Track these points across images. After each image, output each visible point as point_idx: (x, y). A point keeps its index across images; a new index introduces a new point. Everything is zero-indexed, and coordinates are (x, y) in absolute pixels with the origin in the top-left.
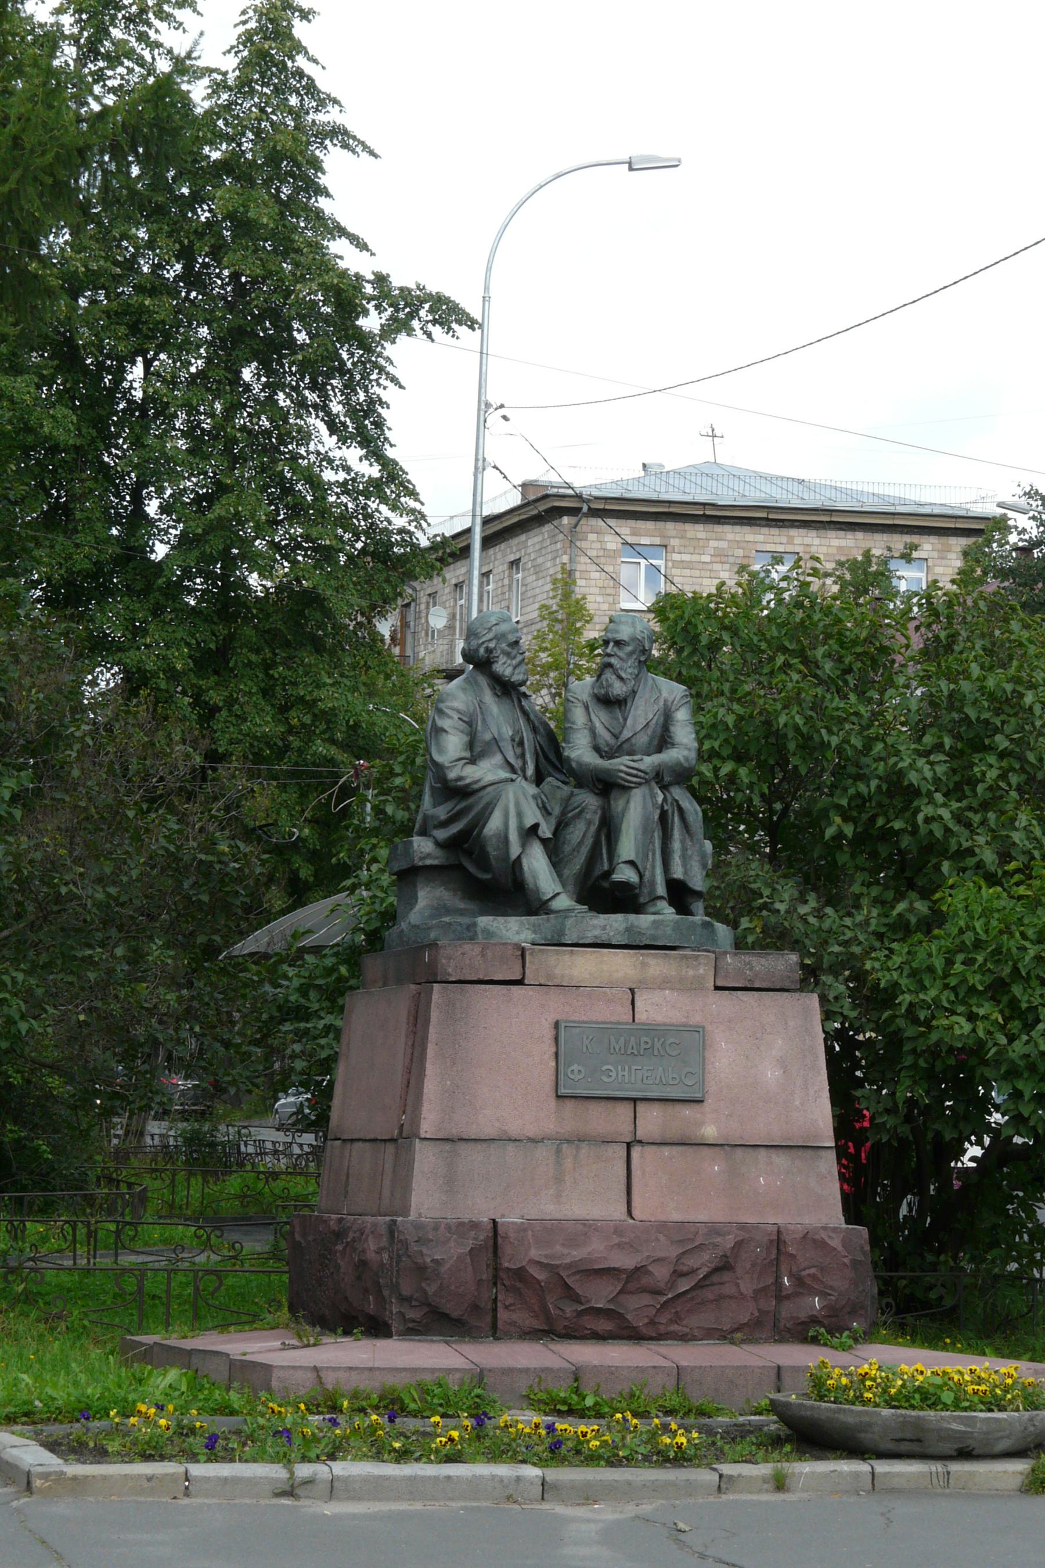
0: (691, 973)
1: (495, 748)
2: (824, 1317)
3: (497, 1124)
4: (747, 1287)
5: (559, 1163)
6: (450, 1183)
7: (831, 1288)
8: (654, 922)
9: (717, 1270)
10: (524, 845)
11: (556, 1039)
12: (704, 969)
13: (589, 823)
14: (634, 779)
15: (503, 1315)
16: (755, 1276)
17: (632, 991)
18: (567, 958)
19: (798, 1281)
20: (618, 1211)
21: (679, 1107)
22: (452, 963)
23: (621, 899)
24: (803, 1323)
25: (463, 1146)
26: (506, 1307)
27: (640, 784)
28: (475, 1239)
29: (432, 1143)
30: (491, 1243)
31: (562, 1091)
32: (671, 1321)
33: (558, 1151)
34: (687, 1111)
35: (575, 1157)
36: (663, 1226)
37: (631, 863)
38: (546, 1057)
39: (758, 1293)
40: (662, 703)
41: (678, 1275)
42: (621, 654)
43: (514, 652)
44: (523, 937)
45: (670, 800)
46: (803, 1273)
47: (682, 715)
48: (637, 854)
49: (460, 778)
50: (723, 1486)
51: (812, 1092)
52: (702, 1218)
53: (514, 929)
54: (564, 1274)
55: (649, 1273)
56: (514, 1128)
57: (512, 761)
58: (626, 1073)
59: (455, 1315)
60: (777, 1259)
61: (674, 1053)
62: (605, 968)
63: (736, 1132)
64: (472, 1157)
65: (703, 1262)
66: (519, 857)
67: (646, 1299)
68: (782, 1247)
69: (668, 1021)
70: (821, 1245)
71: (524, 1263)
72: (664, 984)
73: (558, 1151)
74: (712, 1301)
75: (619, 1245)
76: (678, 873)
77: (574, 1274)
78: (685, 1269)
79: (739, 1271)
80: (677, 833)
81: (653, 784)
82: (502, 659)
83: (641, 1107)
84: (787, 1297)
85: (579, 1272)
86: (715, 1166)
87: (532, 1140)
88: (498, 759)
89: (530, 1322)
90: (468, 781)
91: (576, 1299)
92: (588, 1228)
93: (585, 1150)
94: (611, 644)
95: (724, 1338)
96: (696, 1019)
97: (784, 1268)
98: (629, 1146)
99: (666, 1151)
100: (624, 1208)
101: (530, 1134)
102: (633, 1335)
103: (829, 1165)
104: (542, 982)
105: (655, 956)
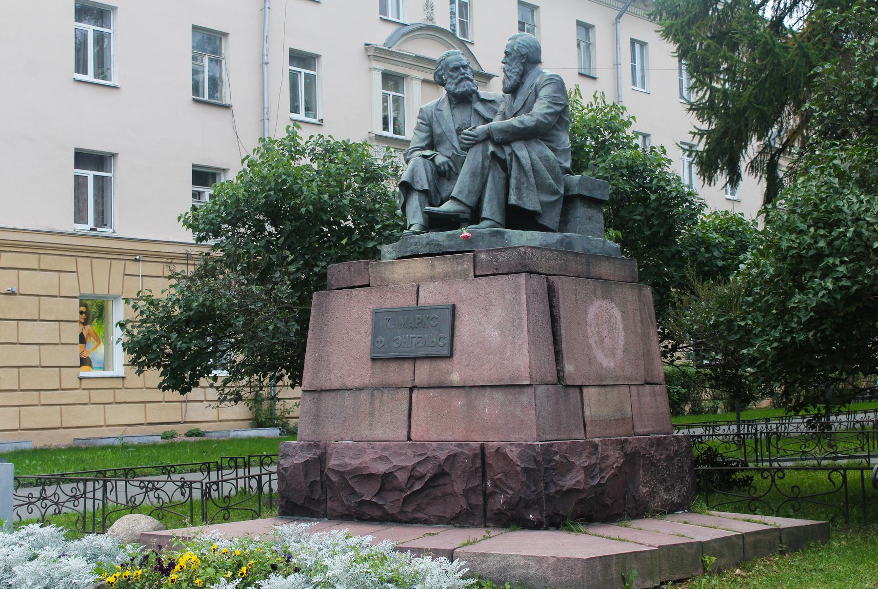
0: (460, 268)
3: (340, 379)
4: (459, 487)
5: (372, 403)
8: (448, 236)
12: (466, 264)
16: (466, 479)
19: (495, 485)
25: (323, 393)
27: (473, 145)
32: (416, 510)
33: (372, 395)
34: (443, 365)
35: (381, 399)
39: (466, 493)
43: (455, 75)
51: (517, 346)
54: (347, 477)
55: (395, 477)
56: (349, 383)
64: (328, 401)
65: (428, 470)
70: (505, 456)
72: (432, 279)
73: (372, 395)
75: (380, 458)
76: (513, 200)
78: (418, 474)
79: (454, 476)
80: (514, 173)
82: (449, 80)
83: (418, 363)
86: (459, 401)
87: (359, 389)
89: (341, 510)
91: (354, 493)
93: (387, 394)
95: (448, 523)
99: (431, 392)
101: (357, 385)
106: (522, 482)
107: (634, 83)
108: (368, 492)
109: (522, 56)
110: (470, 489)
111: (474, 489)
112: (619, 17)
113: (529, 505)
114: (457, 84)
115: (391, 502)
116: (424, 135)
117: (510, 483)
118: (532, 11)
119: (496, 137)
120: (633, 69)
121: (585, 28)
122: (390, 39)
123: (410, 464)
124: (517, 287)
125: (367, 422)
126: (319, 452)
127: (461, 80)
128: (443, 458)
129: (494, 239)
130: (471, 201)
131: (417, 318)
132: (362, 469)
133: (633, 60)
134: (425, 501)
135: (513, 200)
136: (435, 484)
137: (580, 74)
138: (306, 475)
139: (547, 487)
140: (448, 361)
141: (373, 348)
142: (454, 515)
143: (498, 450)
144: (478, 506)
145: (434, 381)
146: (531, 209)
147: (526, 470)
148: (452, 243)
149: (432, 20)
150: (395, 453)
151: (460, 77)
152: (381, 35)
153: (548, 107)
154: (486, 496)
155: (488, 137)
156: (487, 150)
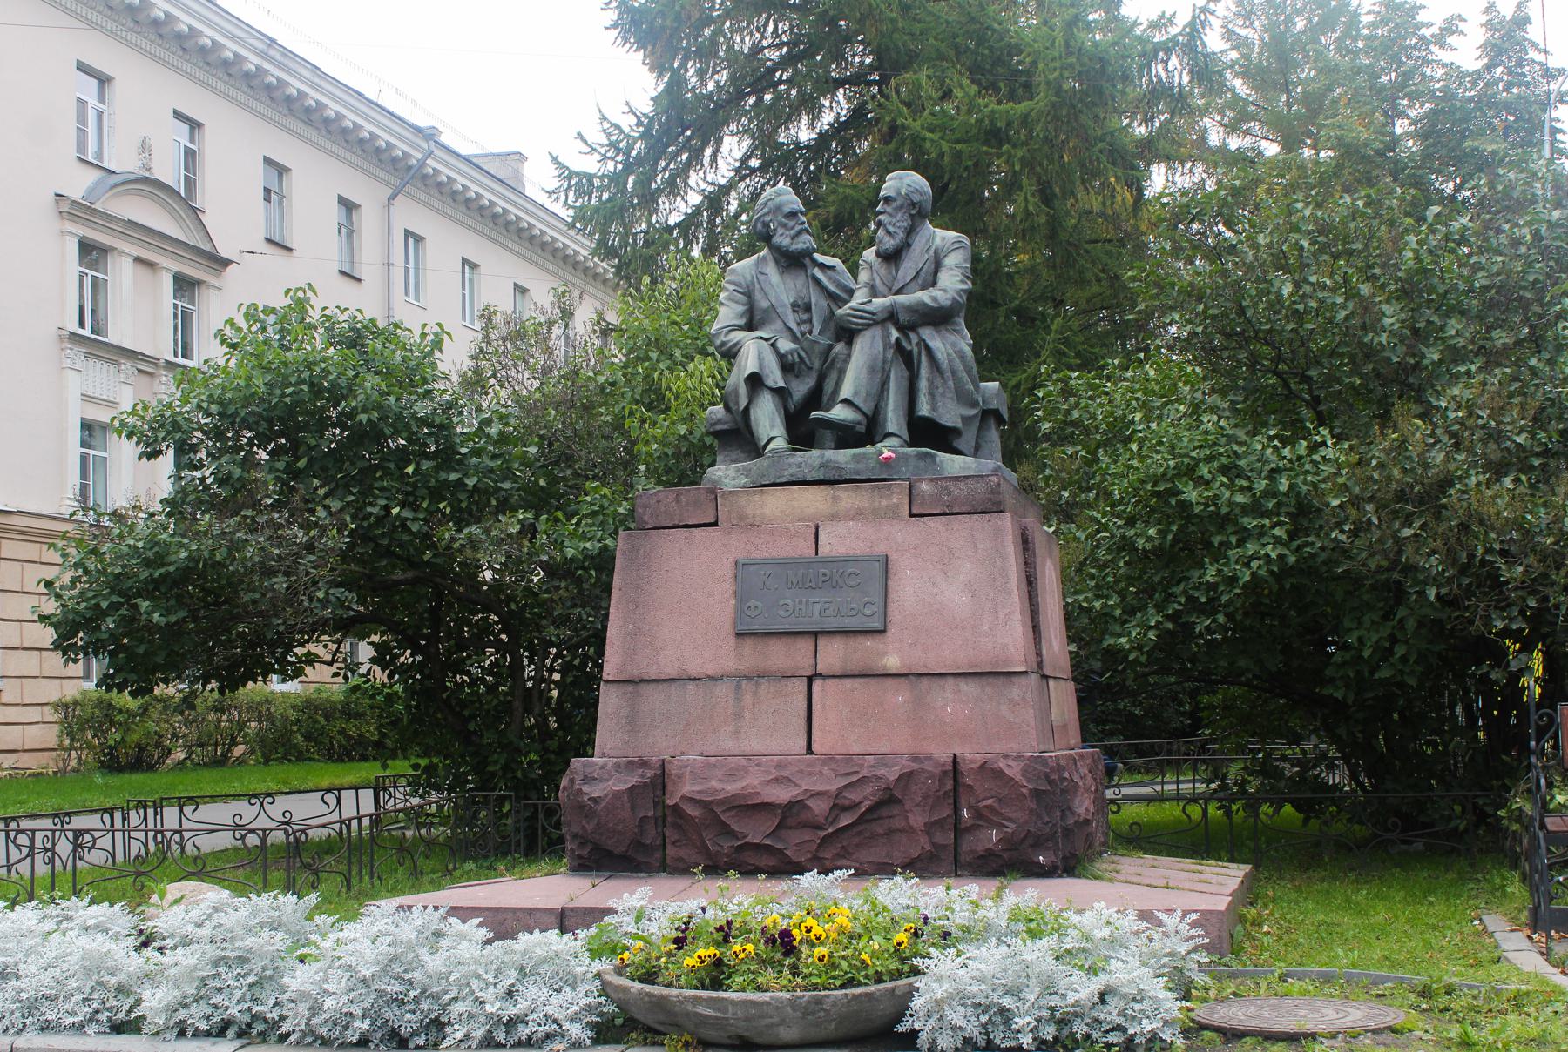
0: (884, 503)
1: (774, 315)
3: (677, 664)
4: (917, 819)
5: (738, 699)
6: (632, 724)
8: (854, 455)
12: (898, 498)
15: (671, 851)
18: (757, 498)
19: (977, 814)
22: (648, 511)
24: (982, 857)
25: (644, 686)
27: (869, 326)
33: (738, 687)
34: (869, 643)
35: (755, 693)
39: (930, 828)
40: (932, 252)
41: (838, 808)
42: (889, 209)
43: (791, 223)
51: (1001, 616)
54: (718, 810)
55: (808, 807)
56: (694, 668)
59: (619, 850)
61: (852, 583)
62: (796, 504)
64: (653, 698)
65: (865, 796)
66: (747, 409)
67: (807, 835)
70: (999, 774)
72: (834, 517)
73: (738, 687)
74: (882, 836)
75: (776, 779)
76: (924, 409)
77: (729, 810)
78: (847, 802)
79: (908, 805)
80: (924, 371)
82: (780, 231)
83: (822, 641)
84: (969, 830)
85: (733, 808)
86: (899, 696)
87: (712, 678)
88: (778, 325)
91: (732, 834)
93: (764, 685)
96: (881, 549)
98: (810, 680)
99: (848, 683)
101: (710, 672)
105: (846, 489)
106: (1031, 811)
107: (407, 293)
108: (756, 832)
109: (913, 205)
110: (936, 822)
111: (939, 823)
112: (393, 197)
113: (1039, 843)
114: (793, 238)
115: (794, 843)
116: (741, 308)
117: (1006, 811)
118: (280, 175)
119: (903, 318)
120: (407, 270)
121: (348, 206)
122: (91, 191)
123: (834, 787)
124: (998, 533)
125: (731, 728)
126: (650, 773)
127: (799, 233)
129: (922, 464)
130: (868, 408)
131: (822, 573)
132: (744, 796)
133: (407, 261)
134: (857, 840)
135: (924, 409)
137: (341, 272)
138: (633, 808)
139: (1063, 817)
140: (878, 637)
141: (740, 613)
143: (983, 766)
144: (945, 846)
145: (852, 667)
146: (950, 424)
147: (1037, 794)
148: (861, 466)
149: (149, 170)
150: (801, 772)
151: (798, 228)
152: (79, 183)
153: (962, 282)
154: (959, 830)
155: (891, 316)
156: (889, 336)
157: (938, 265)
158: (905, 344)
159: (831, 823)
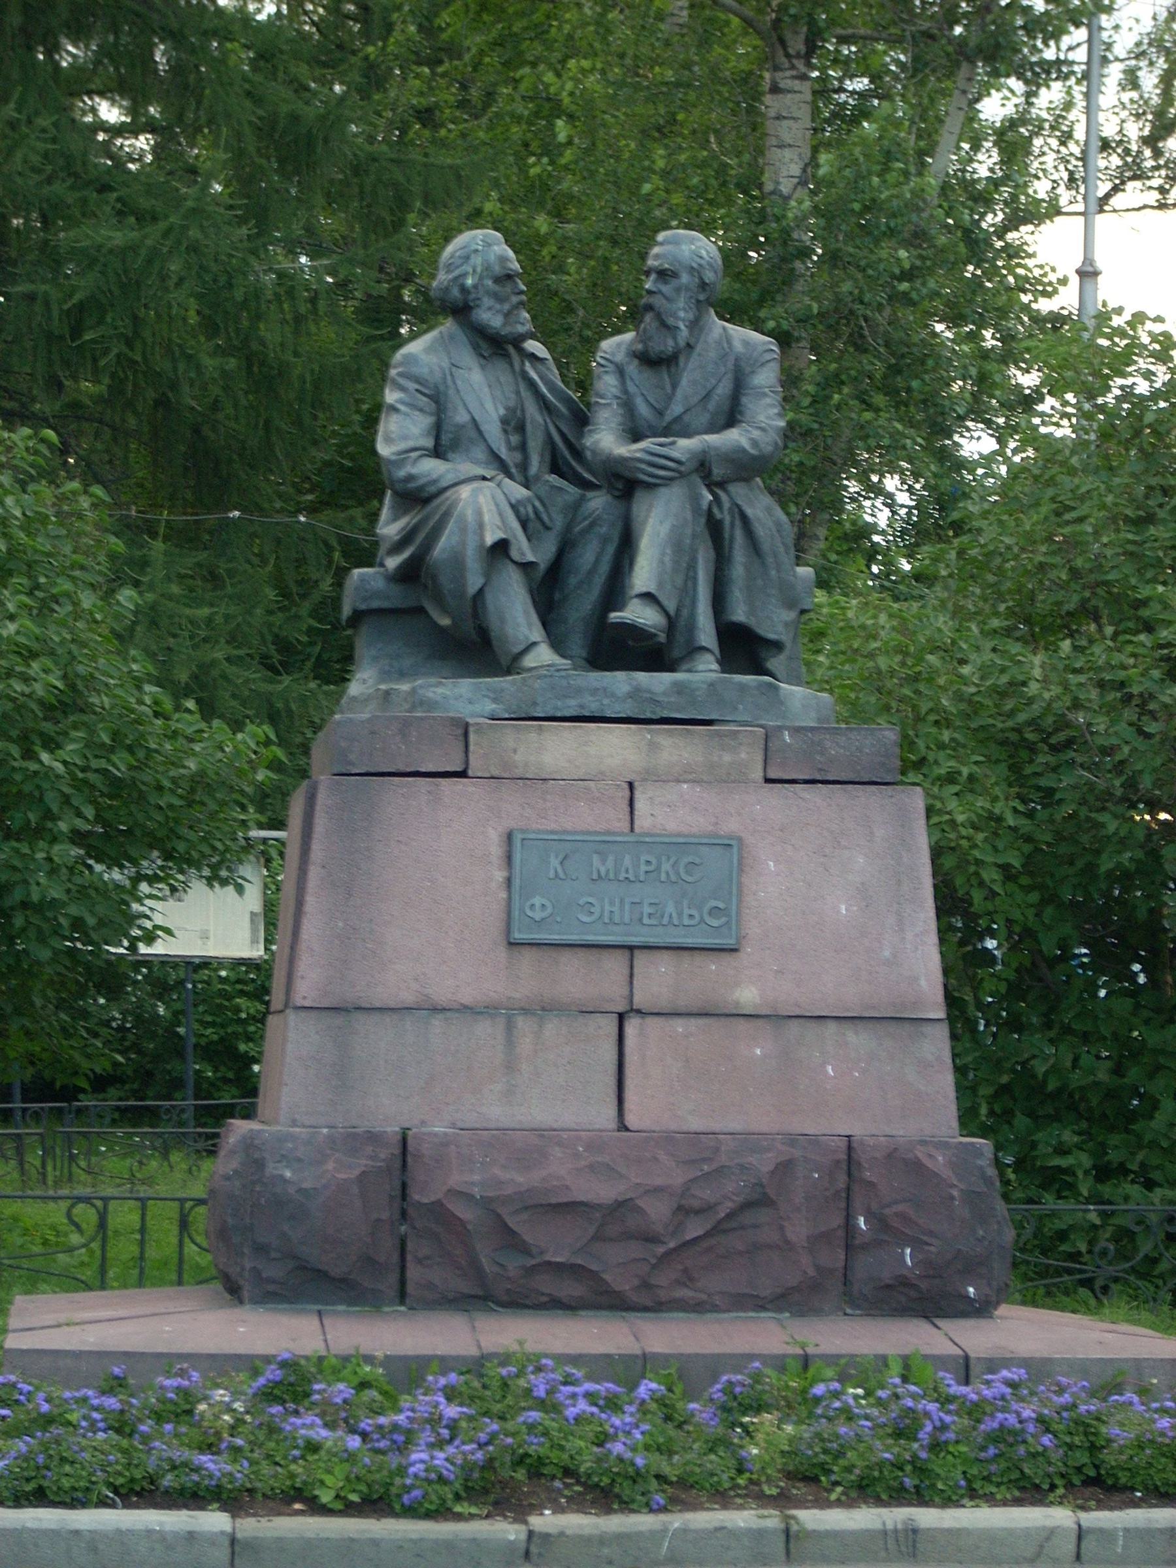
2: (920, 1277)
4: (798, 1231)
7: (931, 1233)
8: (676, 684)
9: (747, 1205)
10: (489, 573)
11: (509, 858)
12: (750, 757)
13: (605, 540)
14: (662, 473)
15: (414, 1273)
17: (631, 785)
18: (533, 736)
19: (879, 1221)
20: (605, 1116)
21: (699, 958)
23: (616, 648)
24: (888, 1286)
25: (360, 1017)
26: (419, 1261)
28: (371, 1158)
29: (313, 1014)
30: (398, 1164)
31: (517, 936)
32: (680, 1283)
33: (510, 1027)
36: (667, 1139)
37: (648, 597)
38: (493, 885)
39: (819, 1239)
44: (477, 708)
45: (726, 504)
46: (887, 1211)
47: (766, 377)
48: (660, 585)
49: (411, 478)
50: (534, 1549)
51: (909, 936)
52: (735, 1125)
53: (463, 695)
54: (503, 1211)
55: (640, 1210)
56: (442, 992)
57: (504, 453)
58: (616, 909)
59: (336, 1272)
60: (848, 1189)
63: (788, 994)
64: (376, 1040)
65: (732, 1191)
66: (481, 591)
67: (635, 1250)
68: (855, 1173)
69: (684, 829)
70: (916, 1168)
71: (440, 1196)
72: (654, 776)
73: (510, 1027)
75: (591, 1167)
76: (739, 614)
78: (696, 1204)
81: (697, 479)
82: (487, 302)
83: (641, 958)
84: (865, 1247)
87: (465, 1009)
90: (421, 482)
91: (524, 1249)
92: (536, 1144)
93: (552, 1028)
94: (653, 276)
96: (731, 826)
97: (858, 1203)
98: (621, 1017)
100: (611, 1111)
101: (467, 1000)
102: (609, 1301)
103: (936, 1045)
104: (496, 773)
108: (558, 1243)
114: (507, 315)
128: (766, 1168)
136: (734, 1224)
140: (726, 958)
142: (779, 1291)
157: (739, 385)
158: (715, 510)
159: (674, 1234)
